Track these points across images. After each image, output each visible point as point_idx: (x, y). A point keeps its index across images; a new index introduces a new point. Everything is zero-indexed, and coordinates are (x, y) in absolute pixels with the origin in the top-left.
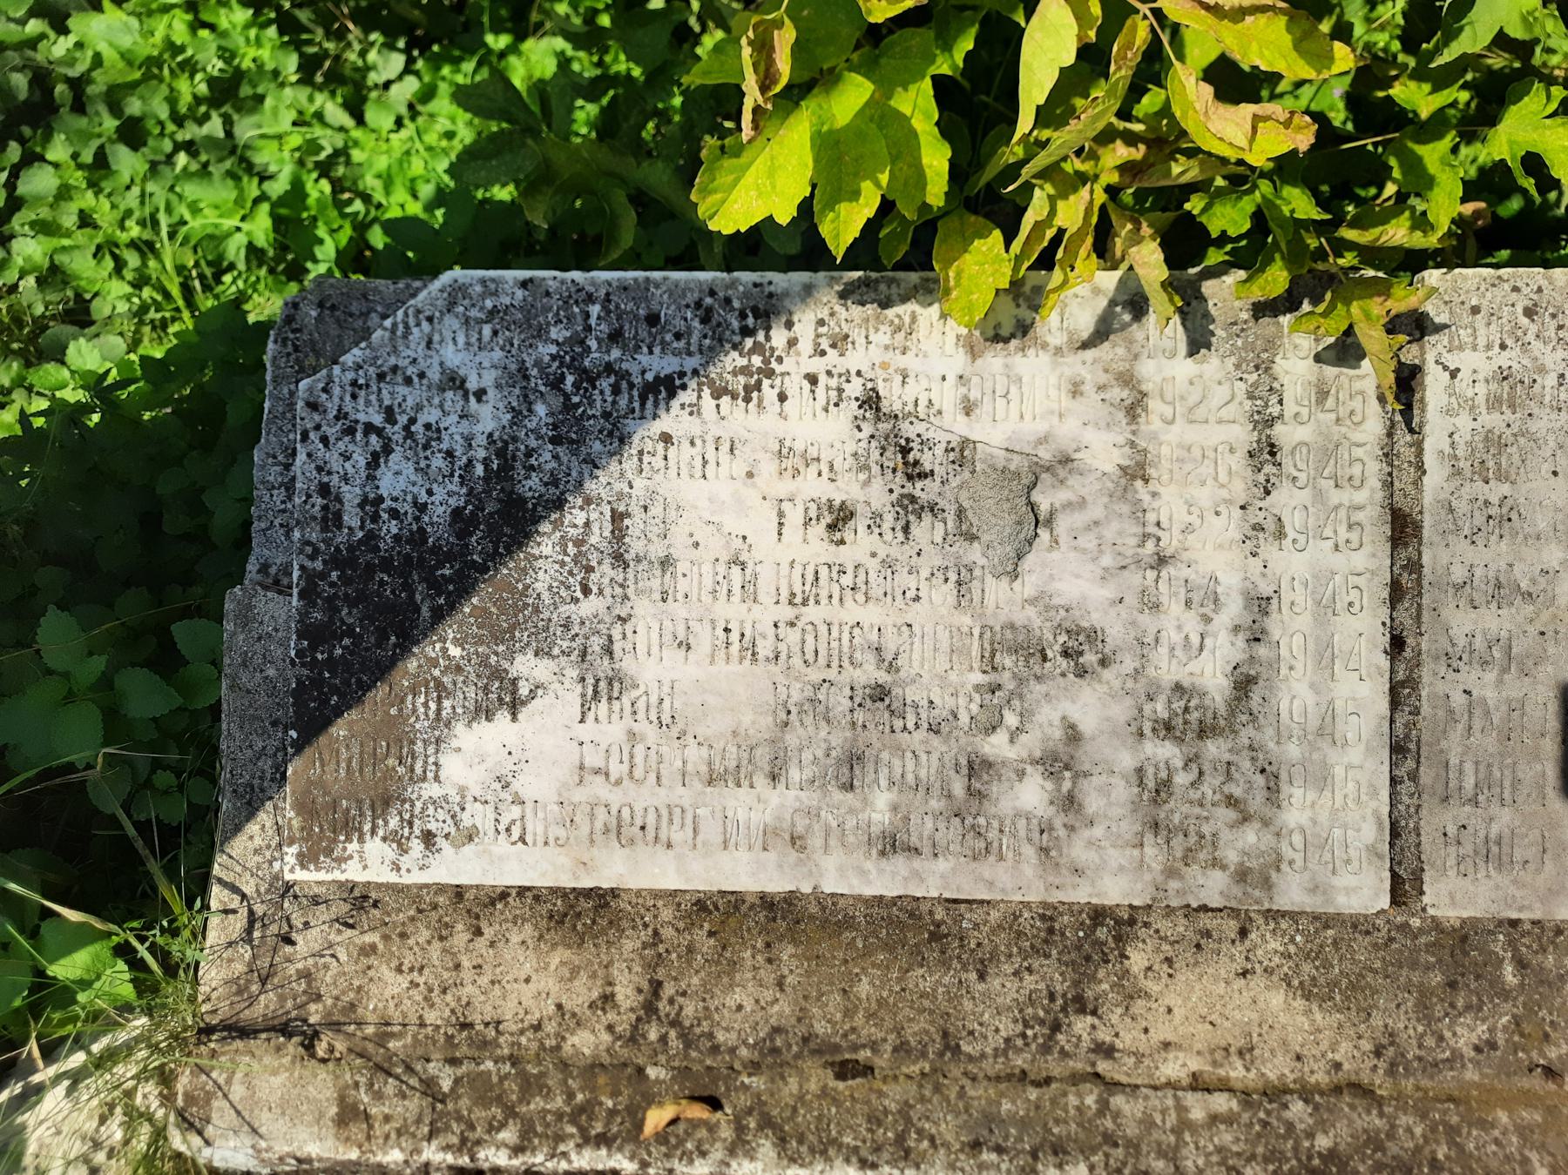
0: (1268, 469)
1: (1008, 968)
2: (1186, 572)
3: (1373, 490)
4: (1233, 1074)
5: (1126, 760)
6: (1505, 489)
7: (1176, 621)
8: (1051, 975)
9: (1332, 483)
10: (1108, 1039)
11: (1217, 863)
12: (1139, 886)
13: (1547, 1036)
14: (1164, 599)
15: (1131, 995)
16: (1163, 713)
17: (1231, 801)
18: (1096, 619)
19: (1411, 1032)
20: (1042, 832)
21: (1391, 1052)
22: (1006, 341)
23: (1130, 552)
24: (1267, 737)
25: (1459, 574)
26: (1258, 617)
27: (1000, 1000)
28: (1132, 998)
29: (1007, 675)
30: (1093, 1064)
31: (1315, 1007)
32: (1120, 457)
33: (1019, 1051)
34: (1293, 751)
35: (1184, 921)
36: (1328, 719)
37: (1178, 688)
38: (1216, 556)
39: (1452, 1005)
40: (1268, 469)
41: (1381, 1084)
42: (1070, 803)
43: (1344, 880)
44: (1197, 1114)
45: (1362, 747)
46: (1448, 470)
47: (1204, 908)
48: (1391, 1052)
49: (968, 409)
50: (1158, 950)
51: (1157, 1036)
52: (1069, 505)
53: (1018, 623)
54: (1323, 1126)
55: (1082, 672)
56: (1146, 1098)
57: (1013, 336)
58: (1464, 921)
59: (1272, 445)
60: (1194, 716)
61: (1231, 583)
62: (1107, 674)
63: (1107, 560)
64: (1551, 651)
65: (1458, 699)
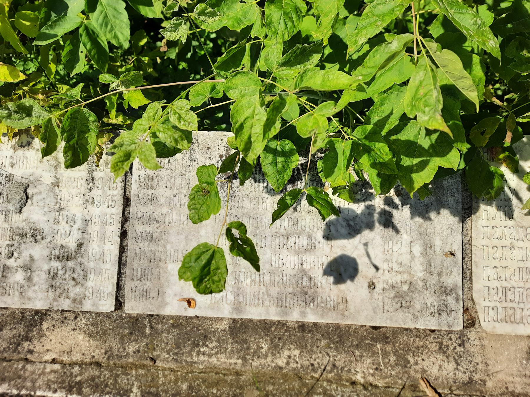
0: (91, 184)
1: (9, 328)
2: (67, 213)
3: (119, 191)
4: (64, 359)
5: (46, 267)
6: (153, 191)
7: (63, 227)
8: (21, 330)
9: (108, 188)
10: (32, 348)
11: (68, 297)
12: (46, 304)
13: (154, 349)
14: (60, 221)
15: (41, 335)
16: (58, 254)
17: (73, 279)
18: (41, 226)
19: (117, 347)
20: (21, 287)
21: (109, 353)
22: (24, 147)
23: (52, 207)
24: (85, 261)
25: (140, 215)
26: (85, 226)
27: (5, 337)
28: (41, 336)
29: (16, 242)
30: (26, 356)
31: (91, 340)
32: (52, 180)
33: (6, 352)
34: (92, 265)
35: (60, 314)
36: (102, 255)
37: (62, 246)
38: (75, 208)
39: (130, 340)
40: (91, 184)
41: (104, 362)
42: (29, 279)
43: (102, 302)
44: (48, 370)
45: (110, 264)
46: (138, 186)
47: (63, 311)
48: (109, 353)
49: (12, 165)
50: (51, 322)
51: (46, 348)
52: (37, 193)
53: (20, 227)
54: (81, 374)
55: (36, 241)
56: (36, 365)
57: (26, 146)
58: (138, 314)
59: (93, 178)
60: (66, 254)
61: (79, 217)
62: (43, 242)
63: (46, 209)
64: (163, 236)
65: (138, 250)
